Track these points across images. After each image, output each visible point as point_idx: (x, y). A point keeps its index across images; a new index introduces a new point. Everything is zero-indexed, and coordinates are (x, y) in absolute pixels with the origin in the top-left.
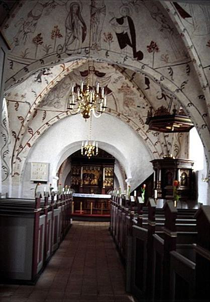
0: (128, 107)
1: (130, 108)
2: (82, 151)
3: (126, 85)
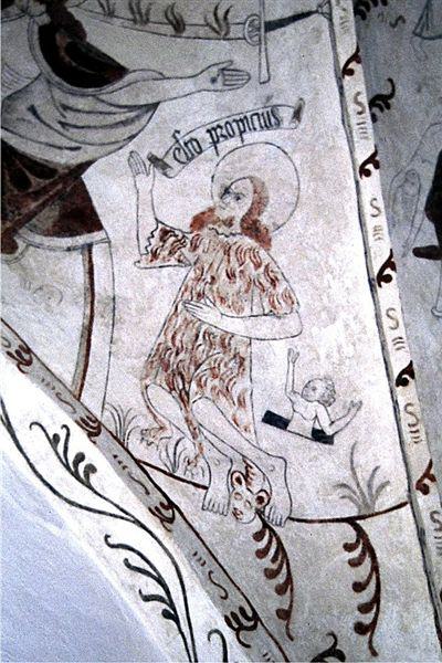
0: (184, 398)
1: (202, 409)
2: (9, 499)
3: (238, 211)
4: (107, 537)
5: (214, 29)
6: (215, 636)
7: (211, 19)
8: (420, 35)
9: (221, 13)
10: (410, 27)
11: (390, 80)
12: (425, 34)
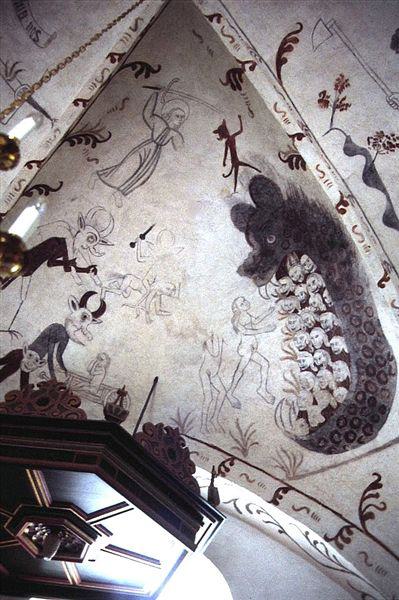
4: (293, 507)
5: (6, 71)
6: (299, 26)
7: (10, 65)
8: (99, 176)
9: (15, 69)
10: (98, 167)
11: (62, 183)
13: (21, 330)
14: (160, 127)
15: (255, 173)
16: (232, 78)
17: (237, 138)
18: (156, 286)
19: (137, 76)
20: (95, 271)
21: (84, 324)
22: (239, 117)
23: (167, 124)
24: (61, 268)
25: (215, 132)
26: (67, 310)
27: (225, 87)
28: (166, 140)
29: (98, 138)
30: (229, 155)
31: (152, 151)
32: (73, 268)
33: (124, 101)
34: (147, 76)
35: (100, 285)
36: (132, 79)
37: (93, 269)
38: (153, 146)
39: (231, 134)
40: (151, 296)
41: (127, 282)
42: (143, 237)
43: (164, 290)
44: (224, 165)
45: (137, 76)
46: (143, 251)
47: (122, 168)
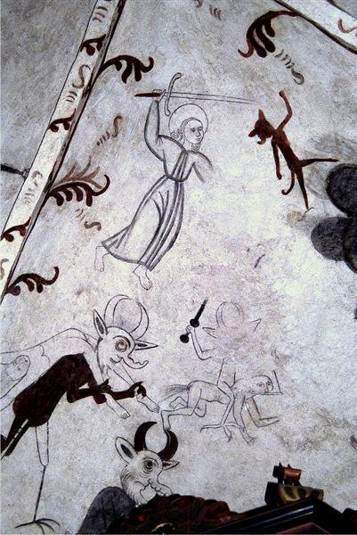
10: (102, 235)
11: (57, 269)
12: (112, 249)
13: (55, 515)
14: (172, 152)
15: (329, 166)
16: (257, 39)
17: (286, 129)
18: (240, 387)
19: (124, 78)
20: (143, 391)
21: (153, 476)
22: (281, 94)
23: (182, 146)
24: (90, 400)
25: (252, 135)
26: (118, 462)
27: (248, 60)
28: (186, 173)
29: (93, 187)
30: (282, 160)
31: (172, 194)
32: (108, 396)
33: (115, 121)
34: (138, 78)
35: (158, 409)
36: (119, 85)
37: (137, 389)
38: (171, 183)
39: (276, 127)
40: (239, 401)
41: (194, 391)
42: (195, 323)
43: (258, 389)
44: (279, 176)
45: (124, 78)
46: (201, 342)
47: (137, 229)
